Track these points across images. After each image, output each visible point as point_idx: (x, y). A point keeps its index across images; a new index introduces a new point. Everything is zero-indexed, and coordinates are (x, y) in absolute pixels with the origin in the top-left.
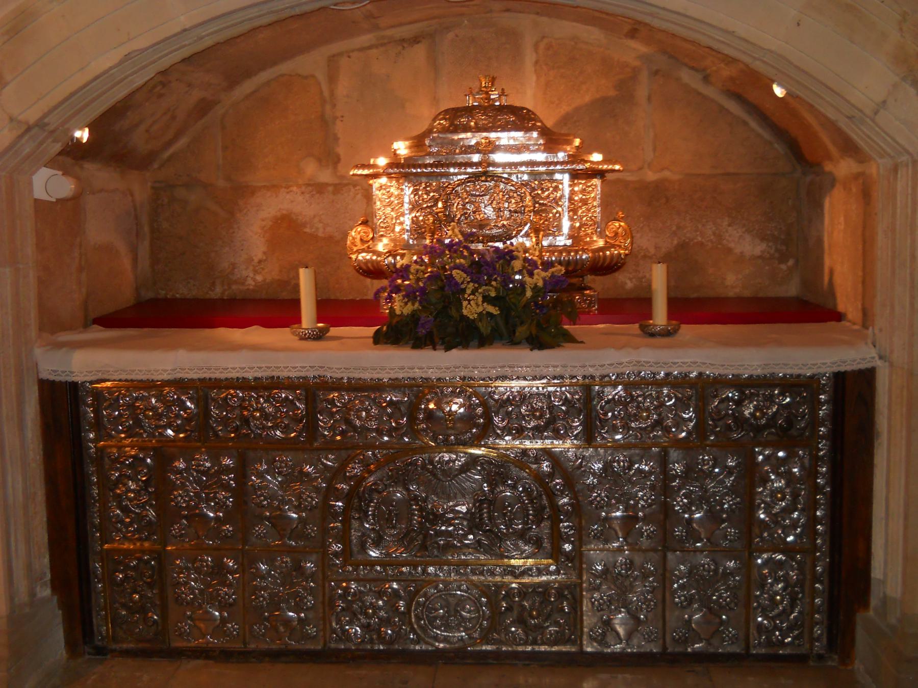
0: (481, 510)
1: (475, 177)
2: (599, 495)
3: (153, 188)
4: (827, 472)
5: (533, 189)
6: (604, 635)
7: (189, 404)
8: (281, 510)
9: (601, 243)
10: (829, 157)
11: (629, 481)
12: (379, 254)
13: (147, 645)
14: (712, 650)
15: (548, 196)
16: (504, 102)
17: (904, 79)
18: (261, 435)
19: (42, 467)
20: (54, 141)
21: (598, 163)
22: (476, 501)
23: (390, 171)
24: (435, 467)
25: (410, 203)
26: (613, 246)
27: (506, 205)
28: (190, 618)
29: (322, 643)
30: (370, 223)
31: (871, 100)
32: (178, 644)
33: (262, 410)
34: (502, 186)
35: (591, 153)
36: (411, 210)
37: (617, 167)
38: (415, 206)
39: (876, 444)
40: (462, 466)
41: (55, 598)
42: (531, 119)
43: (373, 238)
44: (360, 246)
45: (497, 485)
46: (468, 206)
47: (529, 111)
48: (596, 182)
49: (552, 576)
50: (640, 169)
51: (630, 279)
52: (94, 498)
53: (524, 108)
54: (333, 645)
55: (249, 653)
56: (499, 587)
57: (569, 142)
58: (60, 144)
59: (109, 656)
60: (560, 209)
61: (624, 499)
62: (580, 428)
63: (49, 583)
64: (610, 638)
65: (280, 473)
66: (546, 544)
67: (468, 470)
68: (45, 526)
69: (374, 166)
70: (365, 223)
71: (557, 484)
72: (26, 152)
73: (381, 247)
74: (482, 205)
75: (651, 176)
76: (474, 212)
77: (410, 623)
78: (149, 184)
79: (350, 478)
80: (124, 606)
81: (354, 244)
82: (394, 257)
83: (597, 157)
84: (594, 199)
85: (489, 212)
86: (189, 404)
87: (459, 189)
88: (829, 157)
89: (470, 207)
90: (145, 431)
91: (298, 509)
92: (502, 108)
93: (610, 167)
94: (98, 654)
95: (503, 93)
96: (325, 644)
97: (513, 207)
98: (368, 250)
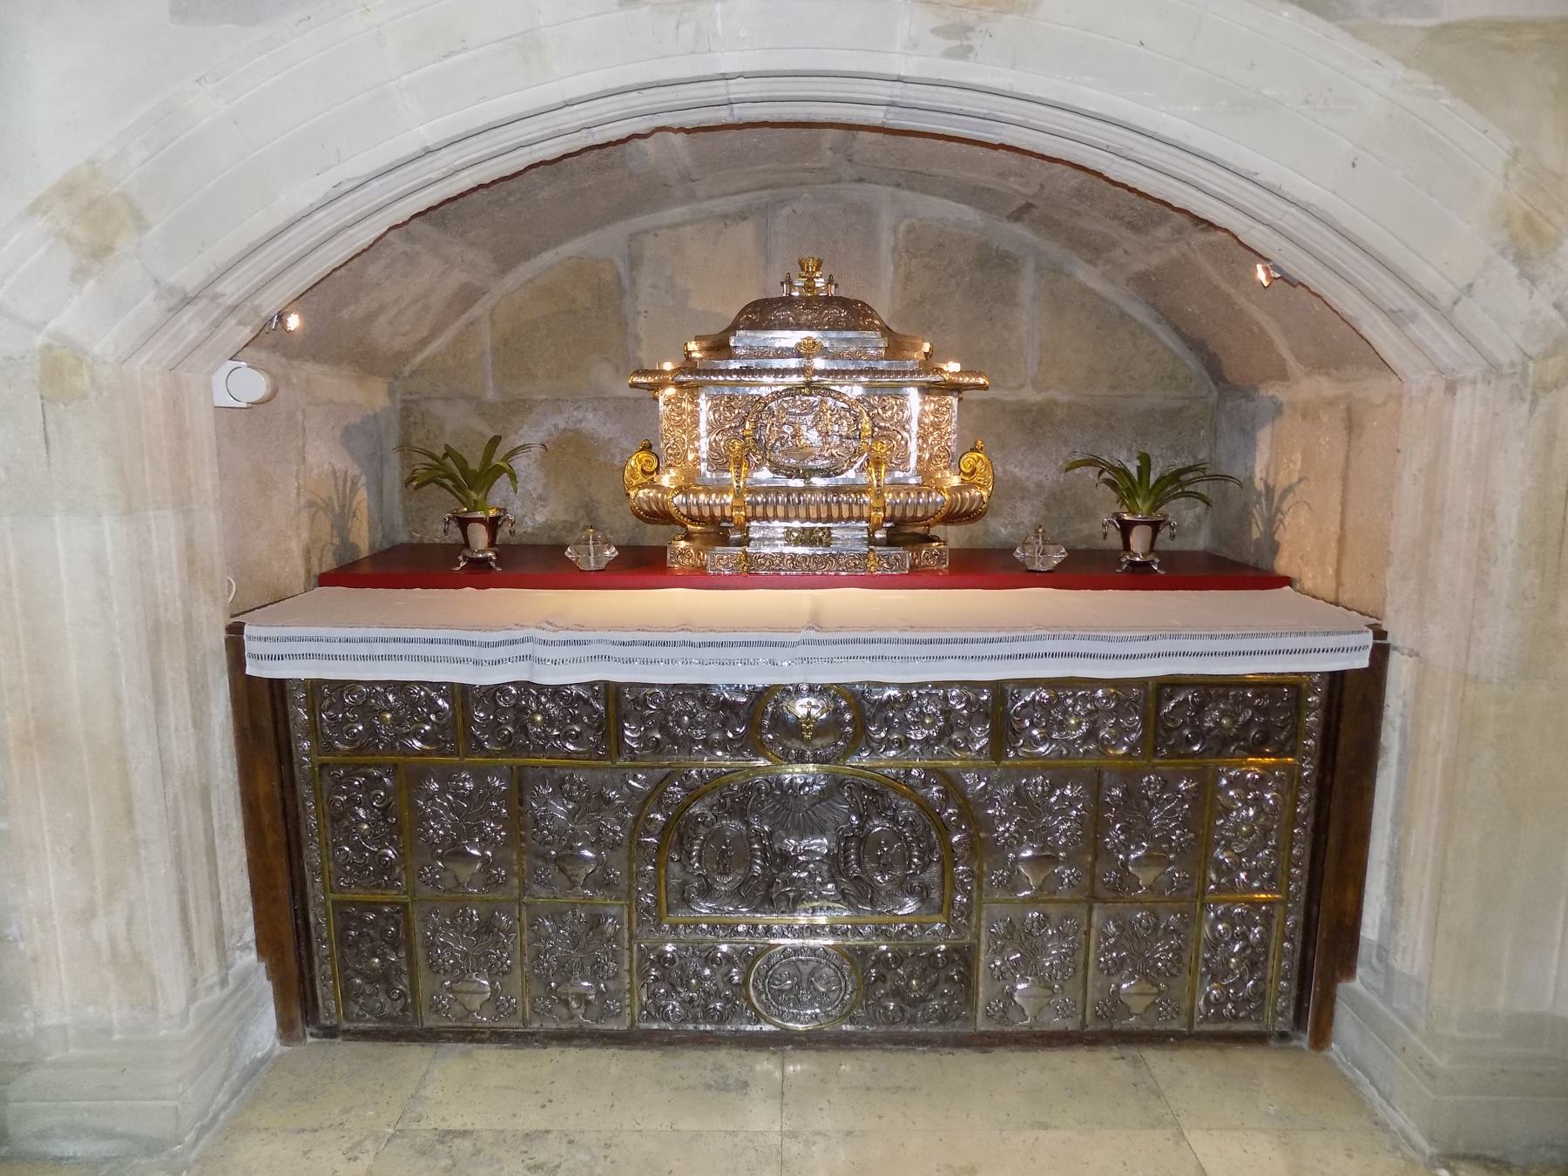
0: (846, 850)
1: (792, 391)
2: (1007, 830)
3: (403, 401)
4: (1310, 799)
5: (873, 407)
6: (1004, 1011)
7: (440, 702)
8: (571, 848)
9: (955, 481)
10: (1282, 375)
11: (1050, 811)
12: (665, 491)
13: (389, 1025)
14: (1145, 1027)
15: (892, 418)
16: (832, 291)
17: (1503, 253)
18: (543, 747)
19: (238, 788)
20: (240, 323)
21: (954, 373)
22: (839, 839)
23: (682, 378)
24: (784, 793)
25: (708, 422)
26: (973, 485)
27: (836, 428)
28: (450, 989)
29: (628, 1022)
30: (654, 449)
31: (1453, 283)
32: (430, 1021)
33: (545, 712)
34: (830, 401)
35: (945, 362)
36: (709, 433)
37: (981, 381)
38: (715, 427)
39: (1380, 763)
40: (822, 791)
41: (263, 965)
42: (866, 316)
43: (657, 469)
44: (641, 479)
45: (869, 817)
46: (785, 428)
47: (864, 304)
48: (953, 400)
49: (939, 936)
50: (1021, 386)
51: (1005, 526)
52: (312, 831)
53: (857, 302)
54: (643, 1025)
55: (532, 1034)
56: (865, 951)
57: (916, 348)
58: (249, 328)
59: (339, 1040)
60: (905, 435)
61: (1040, 834)
62: (985, 741)
63: (253, 945)
64: (1013, 1014)
65: (570, 799)
66: (935, 894)
67: (831, 796)
68: (246, 873)
69: (662, 372)
70: (648, 448)
71: (951, 815)
72: (191, 336)
73: (666, 480)
74: (804, 428)
75: (1031, 395)
76: (794, 437)
77: (748, 998)
78: (398, 396)
79: (668, 807)
80: (359, 973)
81: (633, 476)
82: (686, 494)
83: (953, 367)
84: (949, 422)
85: (813, 436)
86: (440, 702)
87: (773, 405)
88: (1282, 375)
89: (788, 430)
90: (381, 741)
91: (595, 845)
92: (829, 301)
93: (973, 380)
94: (325, 1036)
95: (830, 281)
96: (633, 1022)
97: (845, 430)
98: (652, 485)
